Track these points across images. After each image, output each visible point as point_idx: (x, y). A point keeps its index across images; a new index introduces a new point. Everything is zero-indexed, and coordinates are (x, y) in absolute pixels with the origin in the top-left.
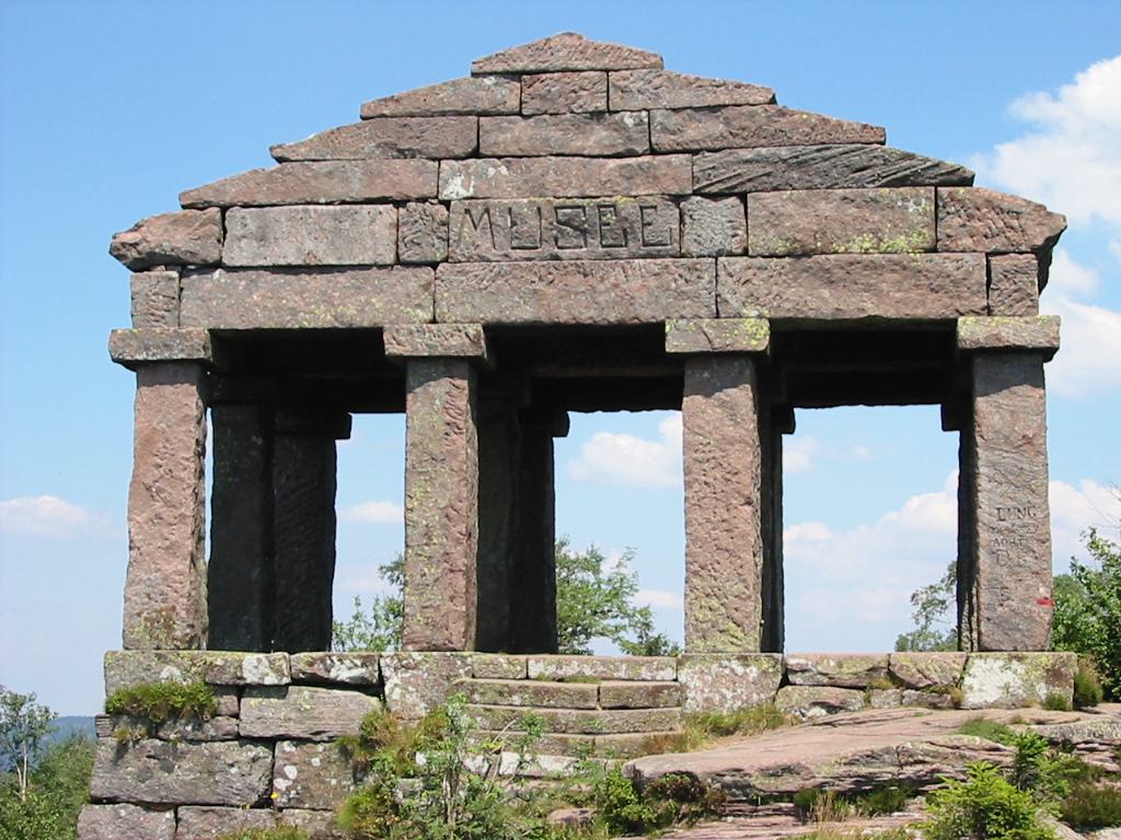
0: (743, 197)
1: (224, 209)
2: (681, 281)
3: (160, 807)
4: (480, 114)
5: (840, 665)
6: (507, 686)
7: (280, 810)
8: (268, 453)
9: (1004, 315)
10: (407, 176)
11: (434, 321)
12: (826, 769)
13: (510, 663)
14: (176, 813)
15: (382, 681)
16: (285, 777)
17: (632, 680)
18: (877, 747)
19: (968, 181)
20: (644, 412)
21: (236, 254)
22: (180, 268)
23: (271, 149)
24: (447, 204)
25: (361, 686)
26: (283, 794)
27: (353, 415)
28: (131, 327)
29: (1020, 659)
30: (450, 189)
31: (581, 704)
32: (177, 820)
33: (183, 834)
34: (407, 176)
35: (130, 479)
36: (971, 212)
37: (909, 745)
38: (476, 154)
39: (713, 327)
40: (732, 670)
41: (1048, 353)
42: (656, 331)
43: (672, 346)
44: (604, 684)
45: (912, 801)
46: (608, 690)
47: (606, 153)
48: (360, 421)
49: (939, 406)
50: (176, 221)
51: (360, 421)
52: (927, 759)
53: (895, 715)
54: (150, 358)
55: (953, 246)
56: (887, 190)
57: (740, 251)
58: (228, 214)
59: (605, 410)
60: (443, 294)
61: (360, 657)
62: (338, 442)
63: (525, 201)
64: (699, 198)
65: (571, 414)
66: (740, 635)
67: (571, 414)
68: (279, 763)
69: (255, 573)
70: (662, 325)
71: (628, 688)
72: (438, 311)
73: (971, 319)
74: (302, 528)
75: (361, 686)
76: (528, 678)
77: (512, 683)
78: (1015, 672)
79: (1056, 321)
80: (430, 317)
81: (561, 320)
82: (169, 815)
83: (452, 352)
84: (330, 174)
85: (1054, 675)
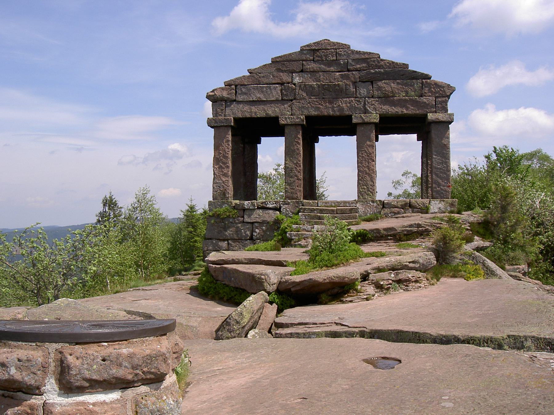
0: (372, 83)
1: (236, 86)
2: (356, 104)
3: (224, 240)
4: (303, 61)
5: (397, 203)
6: (313, 208)
7: (255, 240)
8: (244, 148)
9: (439, 113)
10: (285, 77)
11: (292, 115)
12: (400, 229)
13: (313, 203)
14: (228, 242)
15: (280, 207)
16: (256, 232)
17: (345, 207)
18: (413, 223)
19: (430, 78)
20: (339, 136)
21: (240, 98)
22: (225, 102)
23: (248, 70)
24: (295, 84)
25: (275, 209)
26: (255, 236)
27: (262, 138)
28: (212, 117)
29: (443, 201)
30: (296, 80)
31: (333, 213)
32: (228, 244)
33: (230, 247)
34: (285, 77)
35: (213, 156)
36: (429, 85)
37: (420, 223)
38: (302, 71)
39: (364, 116)
40: (370, 204)
41: (450, 122)
42: (350, 117)
43: (354, 121)
44: (338, 208)
45: (363, 222)
46: (339, 209)
47: (336, 71)
48: (263, 139)
49: (416, 134)
50: (222, 89)
51: (263, 139)
52: (425, 226)
53: (413, 215)
54: (218, 125)
55: (426, 95)
56: (409, 80)
57: (371, 96)
58: (237, 87)
59: (328, 136)
60: (294, 108)
61: (275, 202)
62: (258, 145)
63: (315, 83)
64: (360, 83)
65: (319, 137)
66: (372, 195)
67: (319, 137)
68: (254, 229)
69: (242, 180)
70: (351, 116)
71: (344, 209)
72: (293, 112)
73: (431, 114)
74: (250, 168)
75: (275, 209)
76: (318, 206)
77: (314, 207)
78: (442, 204)
79: (453, 115)
80: (291, 114)
81: (325, 114)
82: (226, 242)
83: (296, 123)
84: (263, 77)
85: (452, 205)
